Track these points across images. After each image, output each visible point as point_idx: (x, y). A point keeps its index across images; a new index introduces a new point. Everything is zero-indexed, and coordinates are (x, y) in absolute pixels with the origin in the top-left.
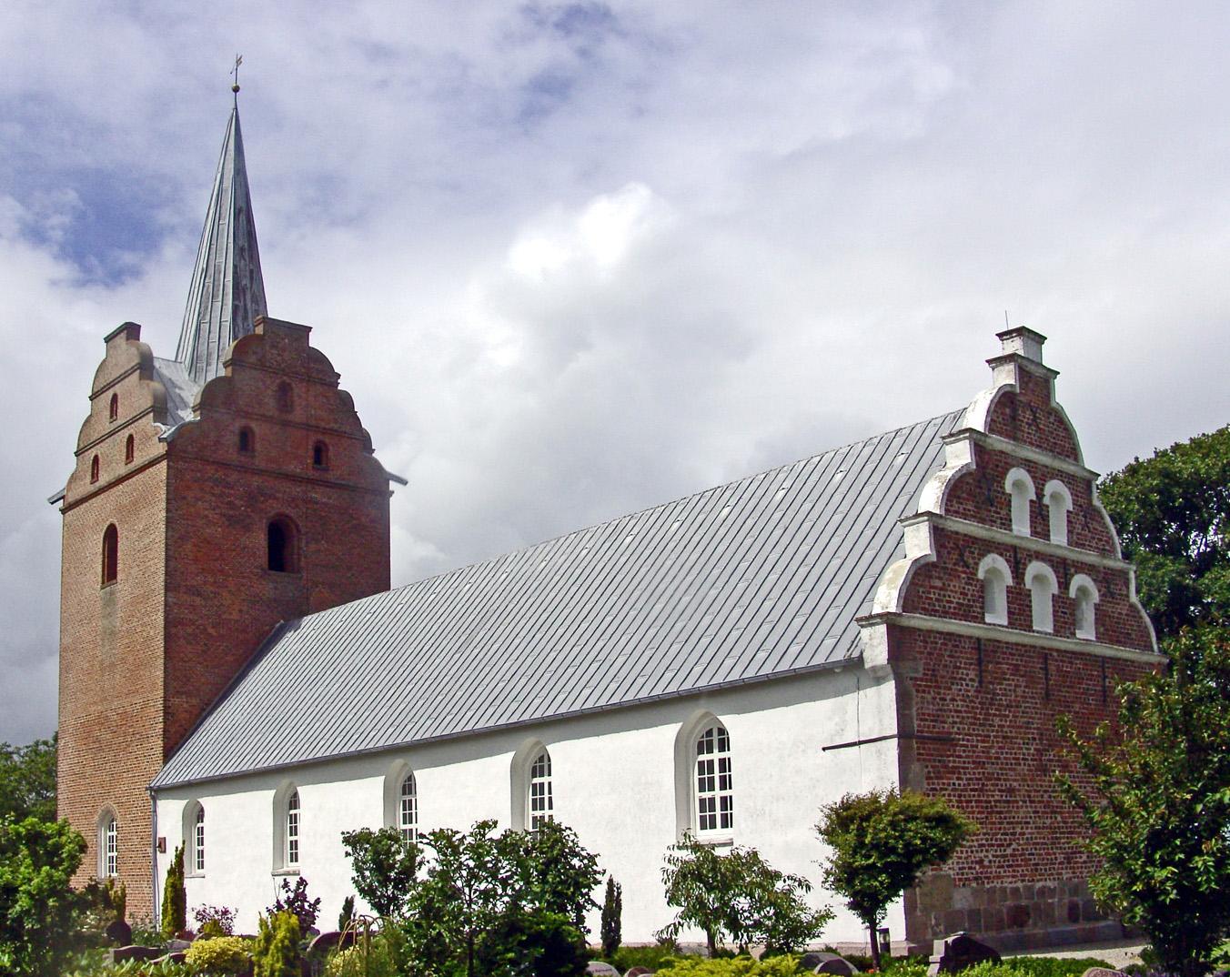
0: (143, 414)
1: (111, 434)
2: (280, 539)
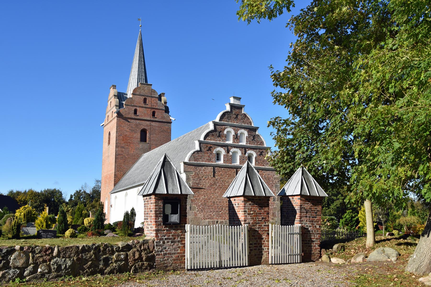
2: (144, 132)
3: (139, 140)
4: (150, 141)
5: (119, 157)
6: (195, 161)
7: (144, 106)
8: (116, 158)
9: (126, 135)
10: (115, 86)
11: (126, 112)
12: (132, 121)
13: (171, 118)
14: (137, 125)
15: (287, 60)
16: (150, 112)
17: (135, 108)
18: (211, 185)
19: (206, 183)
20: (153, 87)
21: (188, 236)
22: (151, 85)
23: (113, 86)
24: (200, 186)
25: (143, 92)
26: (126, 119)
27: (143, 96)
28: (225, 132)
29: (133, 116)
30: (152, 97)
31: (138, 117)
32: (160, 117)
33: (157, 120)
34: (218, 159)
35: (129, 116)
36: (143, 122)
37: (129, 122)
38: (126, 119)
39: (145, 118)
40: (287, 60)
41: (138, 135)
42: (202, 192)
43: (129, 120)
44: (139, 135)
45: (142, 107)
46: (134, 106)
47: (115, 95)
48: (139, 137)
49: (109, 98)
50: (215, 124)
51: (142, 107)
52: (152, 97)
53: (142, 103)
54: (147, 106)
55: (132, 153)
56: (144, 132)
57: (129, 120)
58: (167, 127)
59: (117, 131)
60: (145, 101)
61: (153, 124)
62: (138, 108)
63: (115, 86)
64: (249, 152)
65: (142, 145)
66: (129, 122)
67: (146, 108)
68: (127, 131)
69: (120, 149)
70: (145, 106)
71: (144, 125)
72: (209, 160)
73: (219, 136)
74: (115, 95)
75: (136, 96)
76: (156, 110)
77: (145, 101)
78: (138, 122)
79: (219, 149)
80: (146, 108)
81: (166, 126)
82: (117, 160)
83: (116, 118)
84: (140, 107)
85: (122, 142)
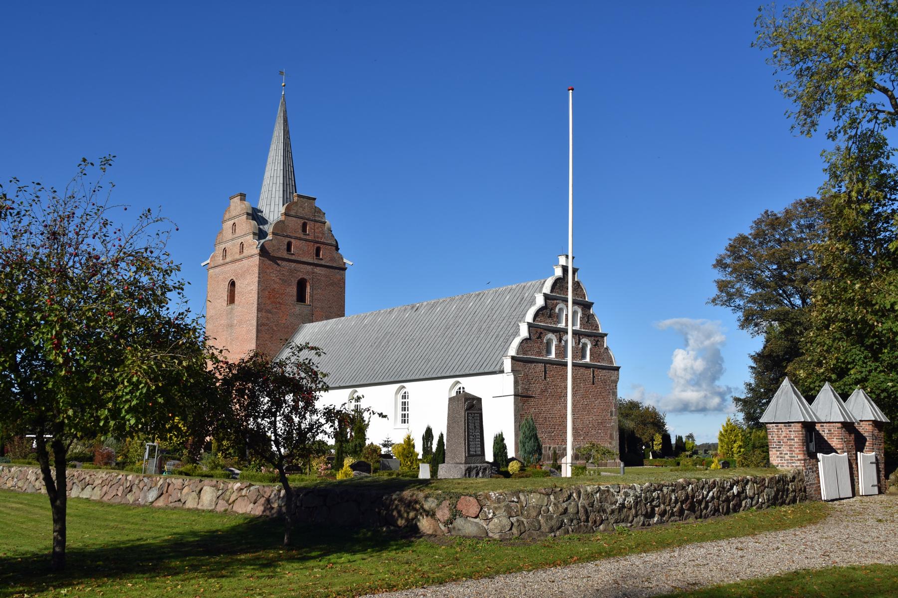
0: (239, 216)
1: (233, 240)
2: (301, 285)
3: (295, 298)
4: (311, 301)
5: (263, 328)
6: (524, 354)
7: (302, 236)
8: (258, 331)
9: (274, 290)
10: (244, 196)
11: (274, 246)
12: (284, 263)
13: (345, 261)
14: (291, 271)
15: (730, 240)
16: (312, 249)
17: (289, 239)
18: (543, 391)
19: (536, 389)
20: (317, 204)
21: (820, 464)
22: (315, 199)
23: (241, 195)
24: (530, 393)
25: (301, 212)
26: (274, 259)
27: (301, 218)
28: (557, 310)
29: (285, 255)
30: (316, 221)
31: (293, 258)
32: (328, 259)
33: (323, 263)
34: (549, 352)
35: (279, 255)
36: (302, 266)
37: (278, 265)
38: (274, 259)
39: (304, 260)
40: (730, 240)
41: (293, 290)
42: (532, 402)
43: (279, 262)
44: (295, 290)
45: (300, 239)
46: (287, 236)
47: (248, 214)
48: (295, 294)
49: (227, 217)
50: (546, 297)
51: (300, 239)
52: (316, 221)
53: (300, 231)
54: (307, 237)
55: (284, 321)
56: (301, 285)
57: (279, 262)
58: (338, 276)
59: (259, 282)
60: (304, 226)
61: (318, 270)
62: (293, 240)
63: (244, 196)
64: (583, 340)
65: (298, 308)
66: (278, 265)
67: (306, 240)
68: (275, 282)
69: (264, 314)
70: (305, 237)
71: (303, 271)
72: (539, 353)
73: (550, 316)
74: (248, 214)
75: (290, 218)
76: (321, 246)
77: (304, 226)
78: (293, 265)
79: (550, 336)
80: (306, 240)
81: (336, 274)
82: (260, 335)
83: (257, 259)
84: (296, 238)
85: (268, 302)
